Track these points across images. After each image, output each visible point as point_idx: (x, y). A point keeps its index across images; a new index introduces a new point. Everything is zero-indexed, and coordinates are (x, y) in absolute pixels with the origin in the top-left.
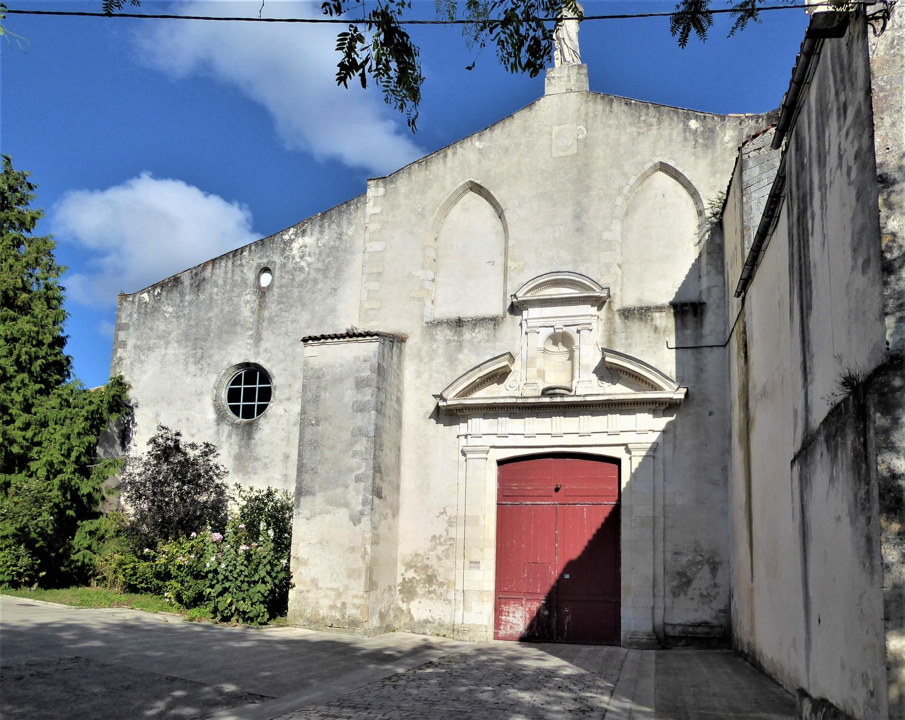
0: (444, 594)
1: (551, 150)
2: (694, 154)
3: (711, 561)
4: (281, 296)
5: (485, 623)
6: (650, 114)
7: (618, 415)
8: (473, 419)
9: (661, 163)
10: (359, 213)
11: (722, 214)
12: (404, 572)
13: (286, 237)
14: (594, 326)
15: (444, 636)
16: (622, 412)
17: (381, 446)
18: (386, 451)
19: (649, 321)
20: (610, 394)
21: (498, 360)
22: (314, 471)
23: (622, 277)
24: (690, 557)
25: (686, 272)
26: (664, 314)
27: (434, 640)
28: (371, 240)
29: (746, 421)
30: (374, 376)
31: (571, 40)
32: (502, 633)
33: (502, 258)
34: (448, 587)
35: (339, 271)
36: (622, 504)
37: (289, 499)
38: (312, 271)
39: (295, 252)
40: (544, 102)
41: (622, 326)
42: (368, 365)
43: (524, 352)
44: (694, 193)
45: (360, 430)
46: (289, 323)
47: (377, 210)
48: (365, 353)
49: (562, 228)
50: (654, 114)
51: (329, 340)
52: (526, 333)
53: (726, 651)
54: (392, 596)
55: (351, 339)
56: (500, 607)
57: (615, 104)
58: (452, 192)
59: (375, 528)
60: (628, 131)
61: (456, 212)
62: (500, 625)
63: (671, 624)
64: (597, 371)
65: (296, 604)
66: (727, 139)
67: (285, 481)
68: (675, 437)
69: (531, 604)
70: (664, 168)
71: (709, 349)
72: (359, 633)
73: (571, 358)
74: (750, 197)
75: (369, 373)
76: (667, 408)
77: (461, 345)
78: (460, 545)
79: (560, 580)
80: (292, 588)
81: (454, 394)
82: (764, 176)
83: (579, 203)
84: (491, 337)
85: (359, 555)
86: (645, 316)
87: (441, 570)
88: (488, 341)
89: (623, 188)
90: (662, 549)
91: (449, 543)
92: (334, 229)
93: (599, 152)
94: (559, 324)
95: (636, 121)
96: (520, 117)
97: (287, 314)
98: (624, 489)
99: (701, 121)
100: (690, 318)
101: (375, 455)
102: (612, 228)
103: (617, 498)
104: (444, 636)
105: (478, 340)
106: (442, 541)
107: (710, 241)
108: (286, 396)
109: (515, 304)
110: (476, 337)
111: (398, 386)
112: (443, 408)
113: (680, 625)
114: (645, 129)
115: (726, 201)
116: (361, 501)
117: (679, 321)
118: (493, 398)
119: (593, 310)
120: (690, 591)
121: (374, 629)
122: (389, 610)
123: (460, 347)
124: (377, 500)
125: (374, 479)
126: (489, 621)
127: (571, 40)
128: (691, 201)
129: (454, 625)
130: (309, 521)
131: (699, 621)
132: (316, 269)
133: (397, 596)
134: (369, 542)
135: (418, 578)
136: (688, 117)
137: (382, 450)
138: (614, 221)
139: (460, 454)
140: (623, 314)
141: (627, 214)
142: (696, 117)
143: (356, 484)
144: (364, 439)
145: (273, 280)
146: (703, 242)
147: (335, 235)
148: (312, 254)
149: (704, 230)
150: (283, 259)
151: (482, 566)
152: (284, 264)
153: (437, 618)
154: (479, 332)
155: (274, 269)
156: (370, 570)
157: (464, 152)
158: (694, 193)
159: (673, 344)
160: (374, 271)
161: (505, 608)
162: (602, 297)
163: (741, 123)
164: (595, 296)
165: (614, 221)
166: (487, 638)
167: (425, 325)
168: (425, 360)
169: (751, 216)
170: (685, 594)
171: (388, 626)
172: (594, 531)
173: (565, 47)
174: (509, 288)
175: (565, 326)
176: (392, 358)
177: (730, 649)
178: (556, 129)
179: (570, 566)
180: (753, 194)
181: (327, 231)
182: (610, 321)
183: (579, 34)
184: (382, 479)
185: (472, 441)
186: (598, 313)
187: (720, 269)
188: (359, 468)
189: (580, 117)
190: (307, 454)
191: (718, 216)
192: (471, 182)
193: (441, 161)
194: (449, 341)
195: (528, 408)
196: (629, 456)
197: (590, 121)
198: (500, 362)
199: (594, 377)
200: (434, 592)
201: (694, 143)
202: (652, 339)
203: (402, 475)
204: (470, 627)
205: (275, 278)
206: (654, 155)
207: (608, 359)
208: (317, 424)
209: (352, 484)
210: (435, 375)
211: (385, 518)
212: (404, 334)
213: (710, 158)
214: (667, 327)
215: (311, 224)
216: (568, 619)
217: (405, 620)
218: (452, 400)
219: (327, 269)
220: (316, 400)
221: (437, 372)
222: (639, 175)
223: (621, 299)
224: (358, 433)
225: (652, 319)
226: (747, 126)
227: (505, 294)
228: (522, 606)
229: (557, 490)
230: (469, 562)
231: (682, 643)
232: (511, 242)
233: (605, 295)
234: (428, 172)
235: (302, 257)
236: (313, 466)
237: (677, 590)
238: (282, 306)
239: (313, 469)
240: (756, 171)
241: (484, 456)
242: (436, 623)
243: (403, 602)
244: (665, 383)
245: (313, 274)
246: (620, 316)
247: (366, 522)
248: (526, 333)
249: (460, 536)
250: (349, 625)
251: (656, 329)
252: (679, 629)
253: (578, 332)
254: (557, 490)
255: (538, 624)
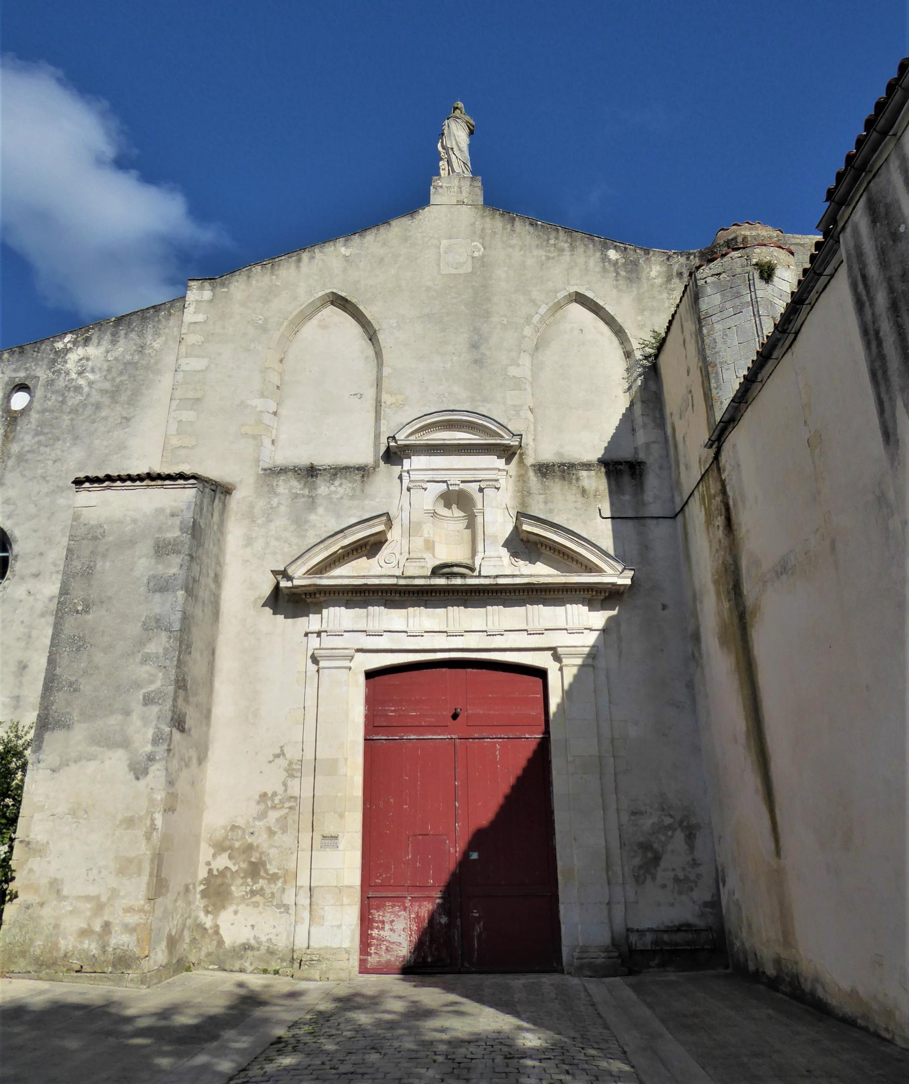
0: (277, 895)
1: (439, 265)
2: (617, 287)
3: (685, 824)
4: (41, 424)
5: (346, 945)
6: (561, 238)
7: (541, 606)
8: (331, 609)
9: (577, 293)
10: (172, 322)
11: (656, 356)
12: (210, 858)
13: (59, 345)
14: (502, 483)
15: (276, 972)
16: (546, 603)
17: (189, 646)
18: (196, 654)
19: (574, 481)
20: (531, 576)
21: (371, 523)
22: (74, 688)
23: (535, 423)
24: (654, 819)
25: (616, 423)
26: (593, 473)
27: (255, 981)
28: (187, 356)
29: (735, 613)
30: (186, 538)
31: (460, 149)
32: (372, 960)
33: (374, 390)
34: (285, 882)
35: (132, 401)
36: (553, 737)
37: (18, 737)
38: (94, 393)
39: (70, 365)
40: (429, 212)
41: (540, 486)
42: (177, 521)
43: (405, 515)
44: (619, 331)
45: (158, 621)
46: (50, 463)
47: (200, 318)
48: (174, 504)
49: (455, 358)
50: (565, 239)
51: (118, 483)
52: (409, 489)
53: (721, 971)
54: (189, 903)
55: (153, 483)
56: (370, 913)
57: (518, 224)
58: (306, 304)
59: (171, 783)
60: (535, 253)
61: (310, 329)
62: (369, 945)
63: (638, 931)
64: (507, 544)
65: (15, 931)
66: (653, 274)
67: (16, 707)
68: (620, 639)
69: (420, 906)
70: (581, 299)
71: (654, 521)
72: (132, 980)
73: (471, 525)
74: (712, 329)
75: (177, 533)
76: (606, 599)
77: (313, 502)
78: (306, 808)
79: (464, 862)
80: (11, 900)
81: (304, 569)
82: (728, 305)
83: (476, 330)
84: (358, 493)
85: (140, 833)
86: (569, 474)
87: (273, 852)
88: (353, 497)
89: (532, 317)
90: (614, 806)
91: (287, 805)
92: (132, 339)
93: (500, 273)
94: (454, 479)
95: (545, 243)
96: (398, 226)
97: (48, 450)
98: (554, 714)
99: (622, 252)
100: (626, 479)
101: (179, 660)
102: (520, 362)
103: (543, 728)
104: (276, 972)
105: (338, 496)
106: (277, 801)
107: (644, 387)
108: (34, 570)
109: (392, 450)
110: (336, 492)
111: (217, 557)
112: (286, 591)
113: (650, 930)
114: (556, 254)
115: (664, 340)
116: (151, 738)
117: (613, 483)
118: (364, 577)
119: (500, 463)
120: (660, 874)
121: (158, 970)
122: (182, 931)
123: (312, 504)
124: (177, 735)
125: (175, 700)
126: (352, 941)
127: (460, 149)
128: (615, 341)
129: (293, 951)
130: (56, 775)
131: (677, 923)
132: (101, 391)
133: (197, 903)
134: (161, 807)
135: (234, 869)
136: (606, 247)
137: (190, 653)
138: (522, 354)
139: (310, 661)
140: (539, 470)
141: (537, 348)
142: (615, 248)
143: (145, 709)
144: (164, 635)
145: (31, 402)
146: (634, 389)
147: (134, 348)
148: (96, 370)
149: (635, 374)
150: (51, 374)
151: (342, 843)
152: (53, 380)
153: (263, 939)
154: (340, 485)
155: (36, 387)
156: (158, 859)
157: (324, 258)
158: (619, 331)
159: (607, 513)
160: (190, 397)
161: (377, 915)
162: (512, 446)
163: (668, 259)
164: (503, 445)
165: (522, 354)
166: (350, 972)
167: (261, 472)
168: (259, 522)
169: (716, 350)
170: (654, 878)
171: (179, 961)
172: (512, 780)
173: (453, 157)
174: (383, 428)
175: (462, 482)
176: (212, 515)
177: (727, 967)
178: (445, 243)
179: (479, 839)
180: (715, 325)
181: (122, 341)
182: (522, 478)
183: (471, 147)
184: (186, 700)
185: (328, 642)
186: (506, 467)
187: (658, 421)
188: (152, 682)
189: (474, 233)
190: (64, 659)
191: (650, 359)
192: (333, 293)
193: (293, 266)
194: (296, 496)
195: (413, 593)
196: (558, 665)
197: (487, 238)
198: (373, 526)
199: (504, 552)
200: (261, 892)
201: (614, 274)
202: (579, 505)
203: (215, 694)
204: (322, 952)
205: (35, 399)
206: (569, 284)
207: (526, 527)
208: (86, 610)
209: (137, 708)
210: (273, 543)
211: (187, 765)
212: (231, 484)
213: (635, 293)
214: (597, 490)
215: (100, 330)
216: (478, 929)
217: (208, 946)
218: (300, 577)
219: (117, 390)
220: (88, 573)
221: (278, 539)
222: (551, 304)
223: (535, 451)
224: (157, 624)
225: (578, 479)
226: (675, 263)
227: (377, 436)
228: (405, 910)
229: (455, 716)
230: (321, 837)
231: (656, 961)
232: (386, 371)
233: (517, 443)
234: (274, 277)
235: (80, 373)
236: (73, 679)
237: (641, 872)
238: (42, 438)
239: (71, 684)
240: (717, 299)
241: (346, 663)
242: (263, 950)
243: (207, 912)
244: (605, 562)
245: (96, 397)
246: (536, 473)
247: (158, 773)
248: (409, 489)
249: (307, 794)
250: (114, 966)
251: (584, 492)
252: (649, 937)
253: (481, 490)
254: (455, 716)
255: (432, 941)
